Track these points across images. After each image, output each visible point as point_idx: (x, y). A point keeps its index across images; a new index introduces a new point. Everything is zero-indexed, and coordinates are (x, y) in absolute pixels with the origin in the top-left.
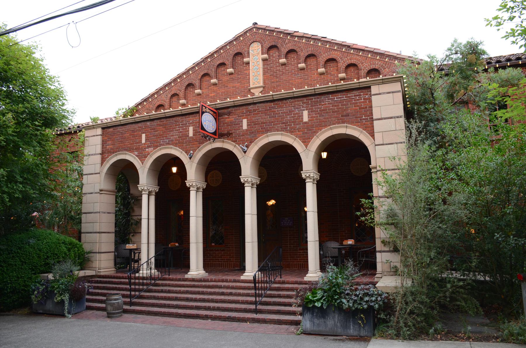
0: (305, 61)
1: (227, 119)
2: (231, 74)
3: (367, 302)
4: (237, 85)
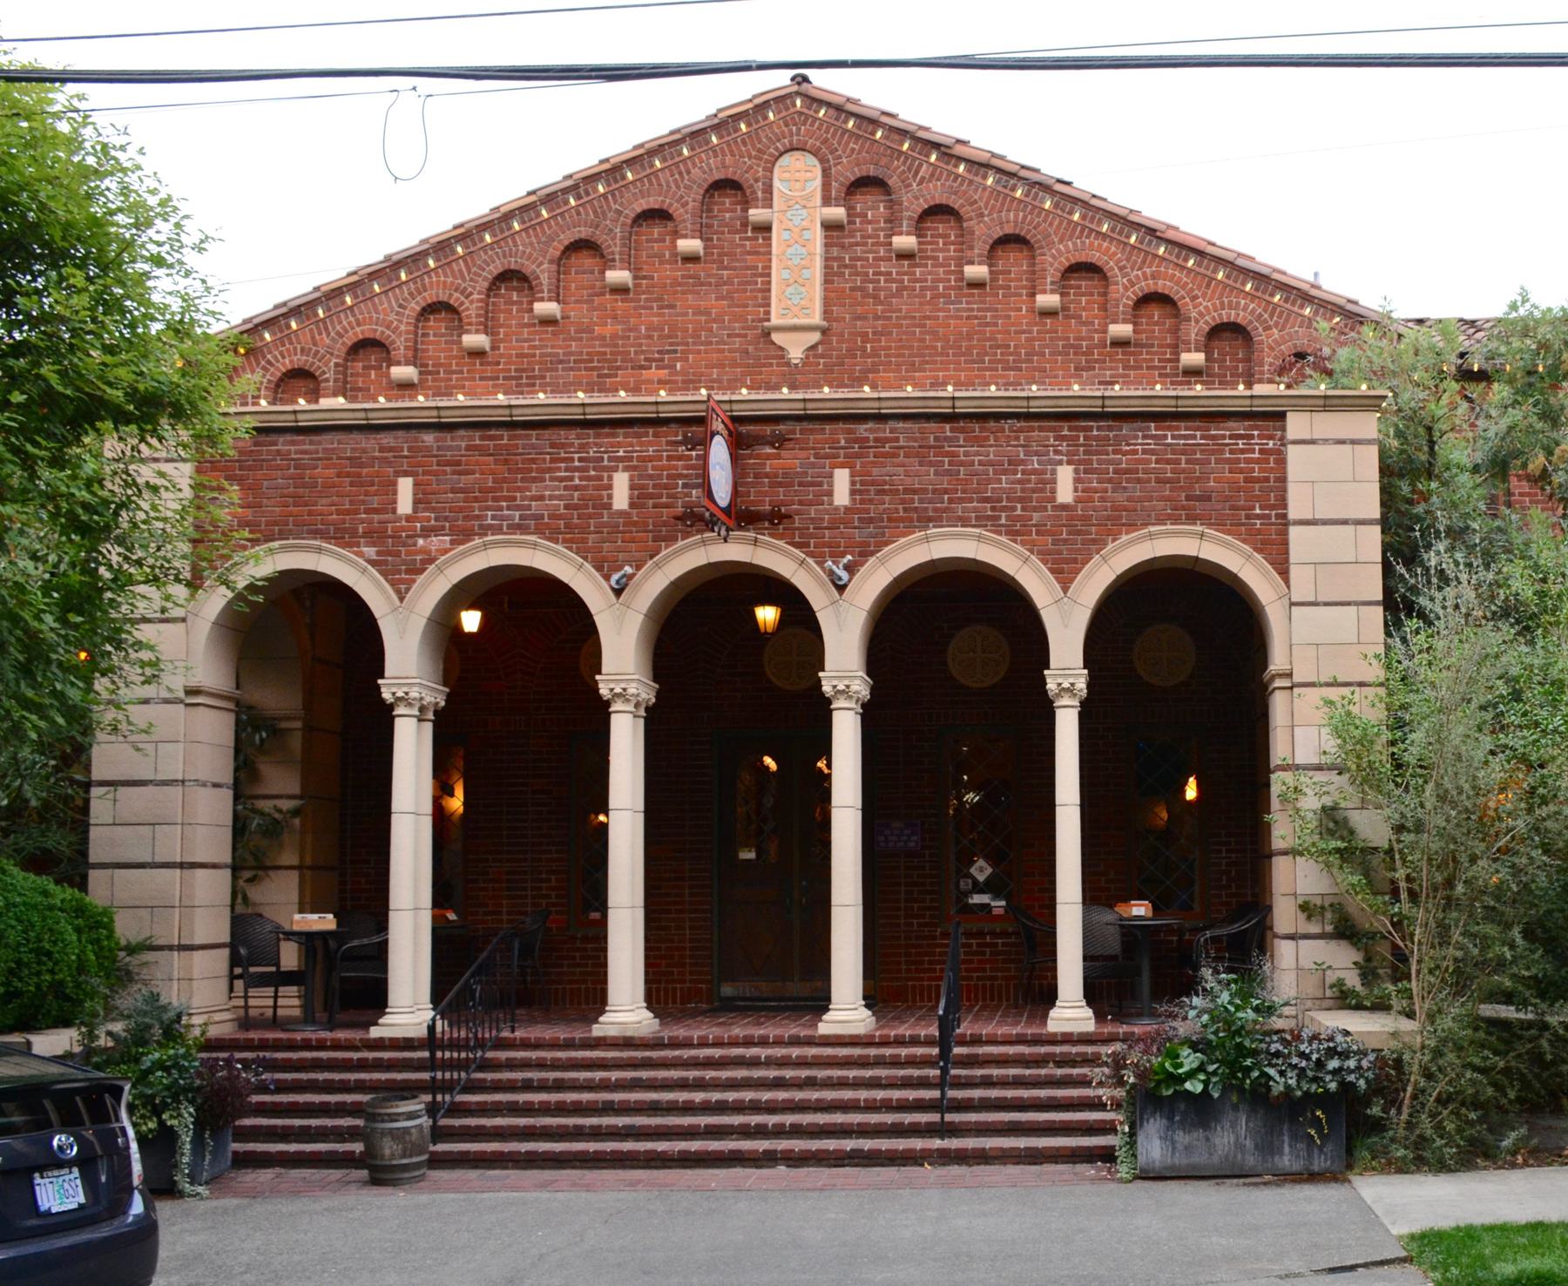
0: (991, 257)
1: (771, 460)
2: (691, 259)
3: (1335, 1072)
4: (711, 302)
